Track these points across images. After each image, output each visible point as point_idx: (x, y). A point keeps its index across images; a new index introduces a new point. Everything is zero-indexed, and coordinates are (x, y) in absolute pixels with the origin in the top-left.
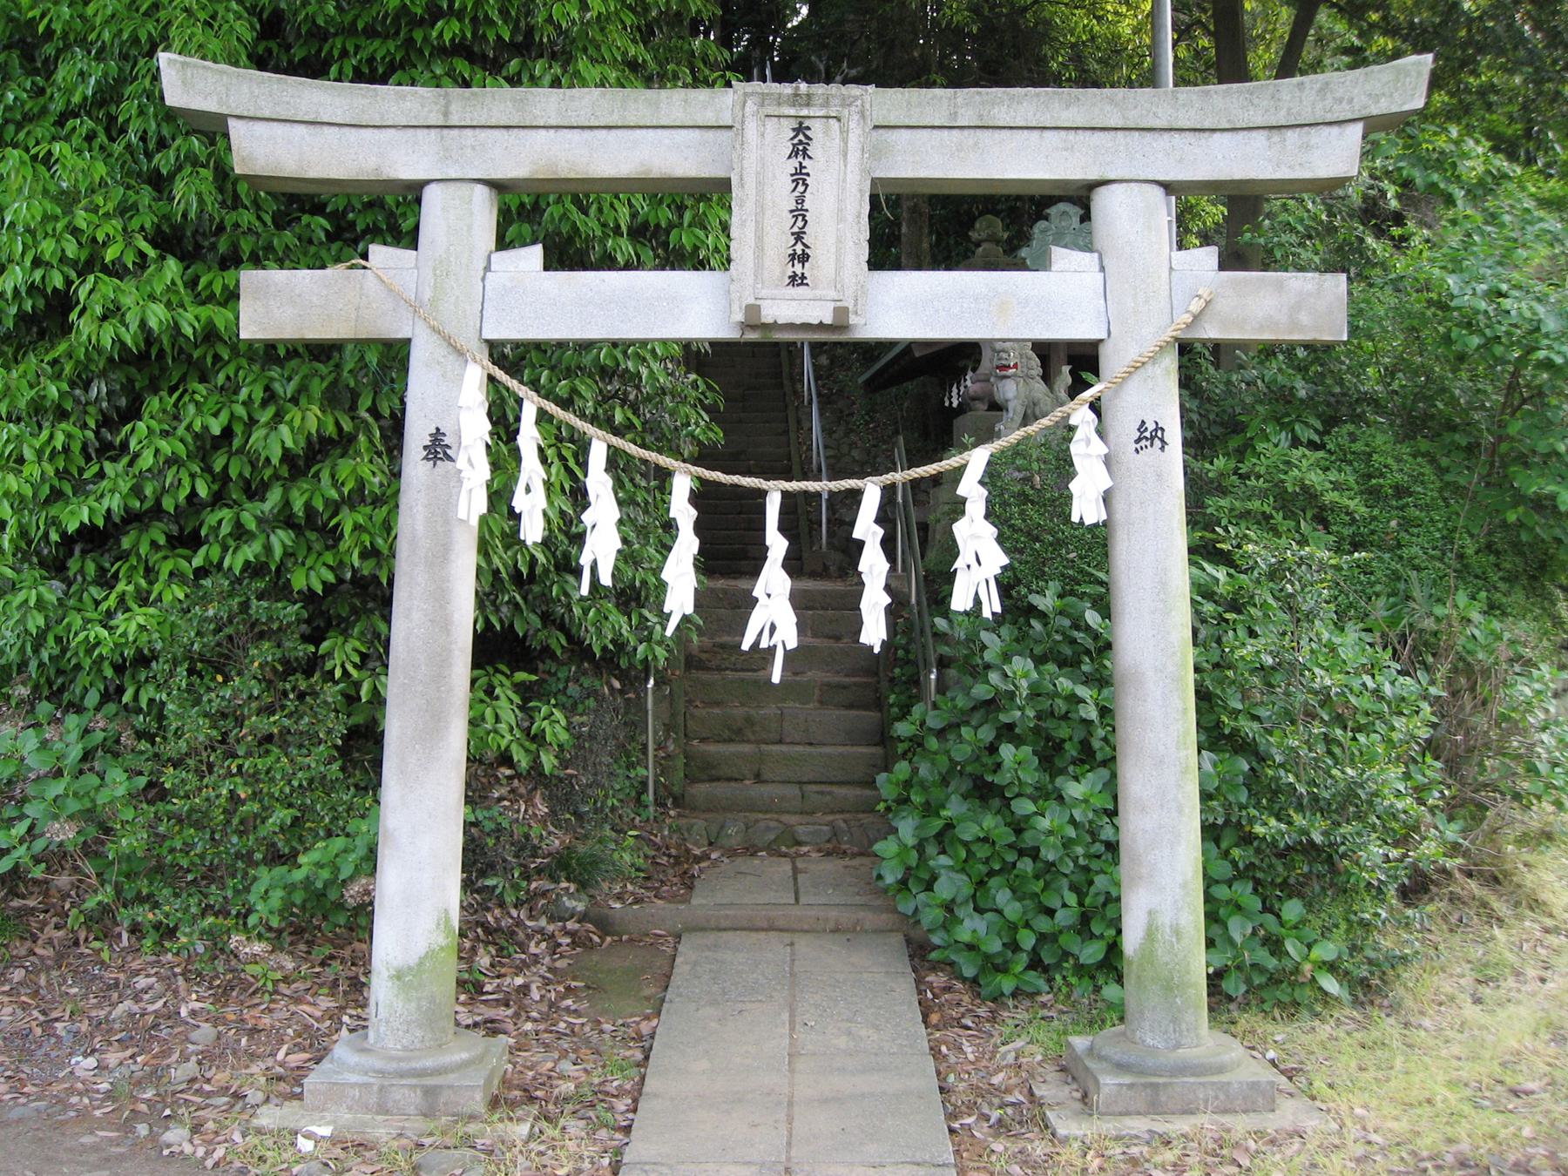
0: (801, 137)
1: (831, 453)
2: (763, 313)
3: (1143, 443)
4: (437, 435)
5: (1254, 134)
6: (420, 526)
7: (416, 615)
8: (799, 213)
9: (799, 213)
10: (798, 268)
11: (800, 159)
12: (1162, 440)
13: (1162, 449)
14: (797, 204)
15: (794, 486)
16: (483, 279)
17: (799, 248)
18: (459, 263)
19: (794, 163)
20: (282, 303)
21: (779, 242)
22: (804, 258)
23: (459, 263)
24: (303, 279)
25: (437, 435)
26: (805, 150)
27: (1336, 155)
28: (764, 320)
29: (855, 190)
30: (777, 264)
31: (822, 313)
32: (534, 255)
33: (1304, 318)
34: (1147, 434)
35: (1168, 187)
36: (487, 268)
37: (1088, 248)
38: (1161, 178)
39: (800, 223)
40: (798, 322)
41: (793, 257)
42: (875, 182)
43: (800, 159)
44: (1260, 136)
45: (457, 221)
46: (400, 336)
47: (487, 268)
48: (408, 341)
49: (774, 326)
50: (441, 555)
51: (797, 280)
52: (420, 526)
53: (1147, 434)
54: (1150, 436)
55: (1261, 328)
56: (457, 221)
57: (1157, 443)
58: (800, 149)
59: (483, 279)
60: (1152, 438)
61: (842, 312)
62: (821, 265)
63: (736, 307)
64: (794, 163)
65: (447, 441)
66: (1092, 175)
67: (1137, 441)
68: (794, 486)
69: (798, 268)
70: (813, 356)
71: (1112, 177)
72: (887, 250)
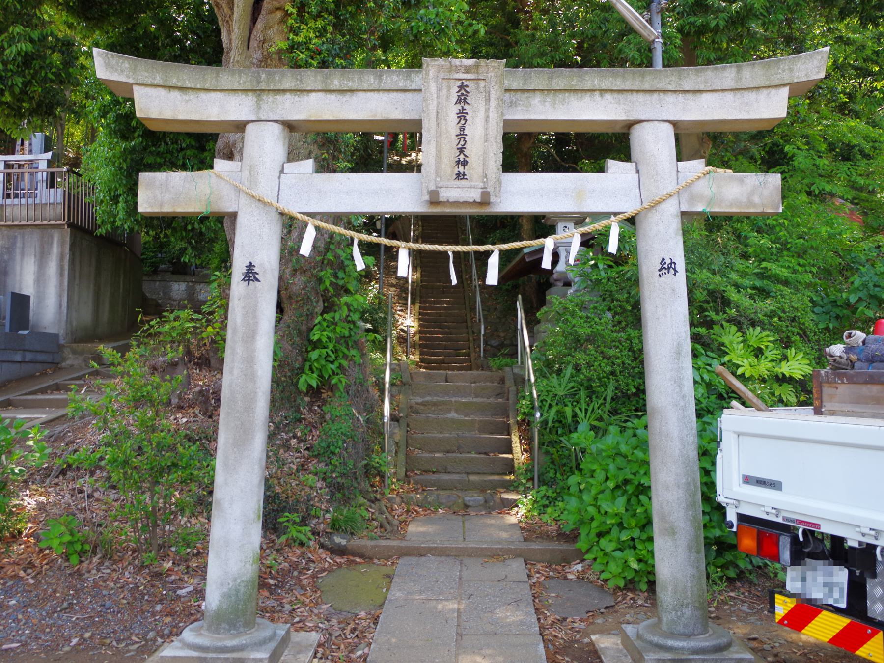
0: (463, 91)
1: (486, 313)
2: (441, 195)
3: (664, 271)
4: (250, 267)
5: (726, 93)
6: (239, 320)
7: (236, 372)
8: (461, 136)
9: (461, 136)
10: (461, 169)
11: (462, 104)
12: (674, 269)
13: (675, 274)
14: (458, 121)
15: (506, 246)
16: (279, 177)
17: (462, 157)
18: (271, 171)
19: (459, 107)
20: (165, 192)
21: (450, 154)
22: (465, 163)
23: (271, 171)
24: (177, 178)
25: (250, 267)
26: (465, 99)
27: (772, 106)
28: (441, 200)
29: (494, 123)
30: (448, 167)
31: (474, 195)
32: (308, 165)
33: (756, 199)
34: (666, 266)
35: (675, 124)
36: (282, 172)
37: (628, 158)
38: (671, 118)
39: (462, 143)
40: (461, 200)
41: (458, 162)
42: (506, 122)
43: (462, 104)
44: (729, 96)
45: (265, 145)
46: (230, 210)
47: (282, 172)
48: (234, 216)
49: (447, 203)
50: (251, 336)
51: (460, 176)
52: (239, 320)
53: (666, 266)
54: (667, 267)
55: (731, 205)
56: (265, 145)
57: (672, 271)
58: (462, 99)
59: (279, 177)
60: (669, 268)
61: (486, 195)
62: (474, 169)
63: (425, 192)
64: (459, 107)
65: (256, 270)
66: (633, 117)
67: (660, 270)
68: (506, 246)
69: (461, 169)
70: (481, 293)
71: (643, 118)
72: (510, 165)
